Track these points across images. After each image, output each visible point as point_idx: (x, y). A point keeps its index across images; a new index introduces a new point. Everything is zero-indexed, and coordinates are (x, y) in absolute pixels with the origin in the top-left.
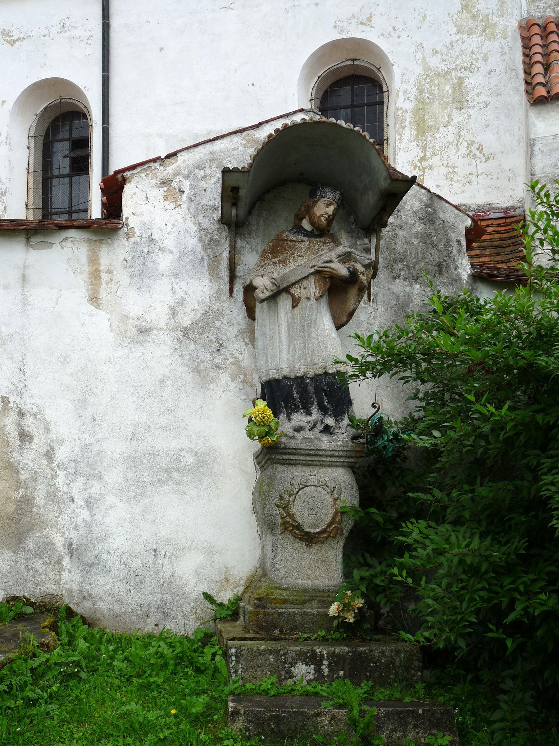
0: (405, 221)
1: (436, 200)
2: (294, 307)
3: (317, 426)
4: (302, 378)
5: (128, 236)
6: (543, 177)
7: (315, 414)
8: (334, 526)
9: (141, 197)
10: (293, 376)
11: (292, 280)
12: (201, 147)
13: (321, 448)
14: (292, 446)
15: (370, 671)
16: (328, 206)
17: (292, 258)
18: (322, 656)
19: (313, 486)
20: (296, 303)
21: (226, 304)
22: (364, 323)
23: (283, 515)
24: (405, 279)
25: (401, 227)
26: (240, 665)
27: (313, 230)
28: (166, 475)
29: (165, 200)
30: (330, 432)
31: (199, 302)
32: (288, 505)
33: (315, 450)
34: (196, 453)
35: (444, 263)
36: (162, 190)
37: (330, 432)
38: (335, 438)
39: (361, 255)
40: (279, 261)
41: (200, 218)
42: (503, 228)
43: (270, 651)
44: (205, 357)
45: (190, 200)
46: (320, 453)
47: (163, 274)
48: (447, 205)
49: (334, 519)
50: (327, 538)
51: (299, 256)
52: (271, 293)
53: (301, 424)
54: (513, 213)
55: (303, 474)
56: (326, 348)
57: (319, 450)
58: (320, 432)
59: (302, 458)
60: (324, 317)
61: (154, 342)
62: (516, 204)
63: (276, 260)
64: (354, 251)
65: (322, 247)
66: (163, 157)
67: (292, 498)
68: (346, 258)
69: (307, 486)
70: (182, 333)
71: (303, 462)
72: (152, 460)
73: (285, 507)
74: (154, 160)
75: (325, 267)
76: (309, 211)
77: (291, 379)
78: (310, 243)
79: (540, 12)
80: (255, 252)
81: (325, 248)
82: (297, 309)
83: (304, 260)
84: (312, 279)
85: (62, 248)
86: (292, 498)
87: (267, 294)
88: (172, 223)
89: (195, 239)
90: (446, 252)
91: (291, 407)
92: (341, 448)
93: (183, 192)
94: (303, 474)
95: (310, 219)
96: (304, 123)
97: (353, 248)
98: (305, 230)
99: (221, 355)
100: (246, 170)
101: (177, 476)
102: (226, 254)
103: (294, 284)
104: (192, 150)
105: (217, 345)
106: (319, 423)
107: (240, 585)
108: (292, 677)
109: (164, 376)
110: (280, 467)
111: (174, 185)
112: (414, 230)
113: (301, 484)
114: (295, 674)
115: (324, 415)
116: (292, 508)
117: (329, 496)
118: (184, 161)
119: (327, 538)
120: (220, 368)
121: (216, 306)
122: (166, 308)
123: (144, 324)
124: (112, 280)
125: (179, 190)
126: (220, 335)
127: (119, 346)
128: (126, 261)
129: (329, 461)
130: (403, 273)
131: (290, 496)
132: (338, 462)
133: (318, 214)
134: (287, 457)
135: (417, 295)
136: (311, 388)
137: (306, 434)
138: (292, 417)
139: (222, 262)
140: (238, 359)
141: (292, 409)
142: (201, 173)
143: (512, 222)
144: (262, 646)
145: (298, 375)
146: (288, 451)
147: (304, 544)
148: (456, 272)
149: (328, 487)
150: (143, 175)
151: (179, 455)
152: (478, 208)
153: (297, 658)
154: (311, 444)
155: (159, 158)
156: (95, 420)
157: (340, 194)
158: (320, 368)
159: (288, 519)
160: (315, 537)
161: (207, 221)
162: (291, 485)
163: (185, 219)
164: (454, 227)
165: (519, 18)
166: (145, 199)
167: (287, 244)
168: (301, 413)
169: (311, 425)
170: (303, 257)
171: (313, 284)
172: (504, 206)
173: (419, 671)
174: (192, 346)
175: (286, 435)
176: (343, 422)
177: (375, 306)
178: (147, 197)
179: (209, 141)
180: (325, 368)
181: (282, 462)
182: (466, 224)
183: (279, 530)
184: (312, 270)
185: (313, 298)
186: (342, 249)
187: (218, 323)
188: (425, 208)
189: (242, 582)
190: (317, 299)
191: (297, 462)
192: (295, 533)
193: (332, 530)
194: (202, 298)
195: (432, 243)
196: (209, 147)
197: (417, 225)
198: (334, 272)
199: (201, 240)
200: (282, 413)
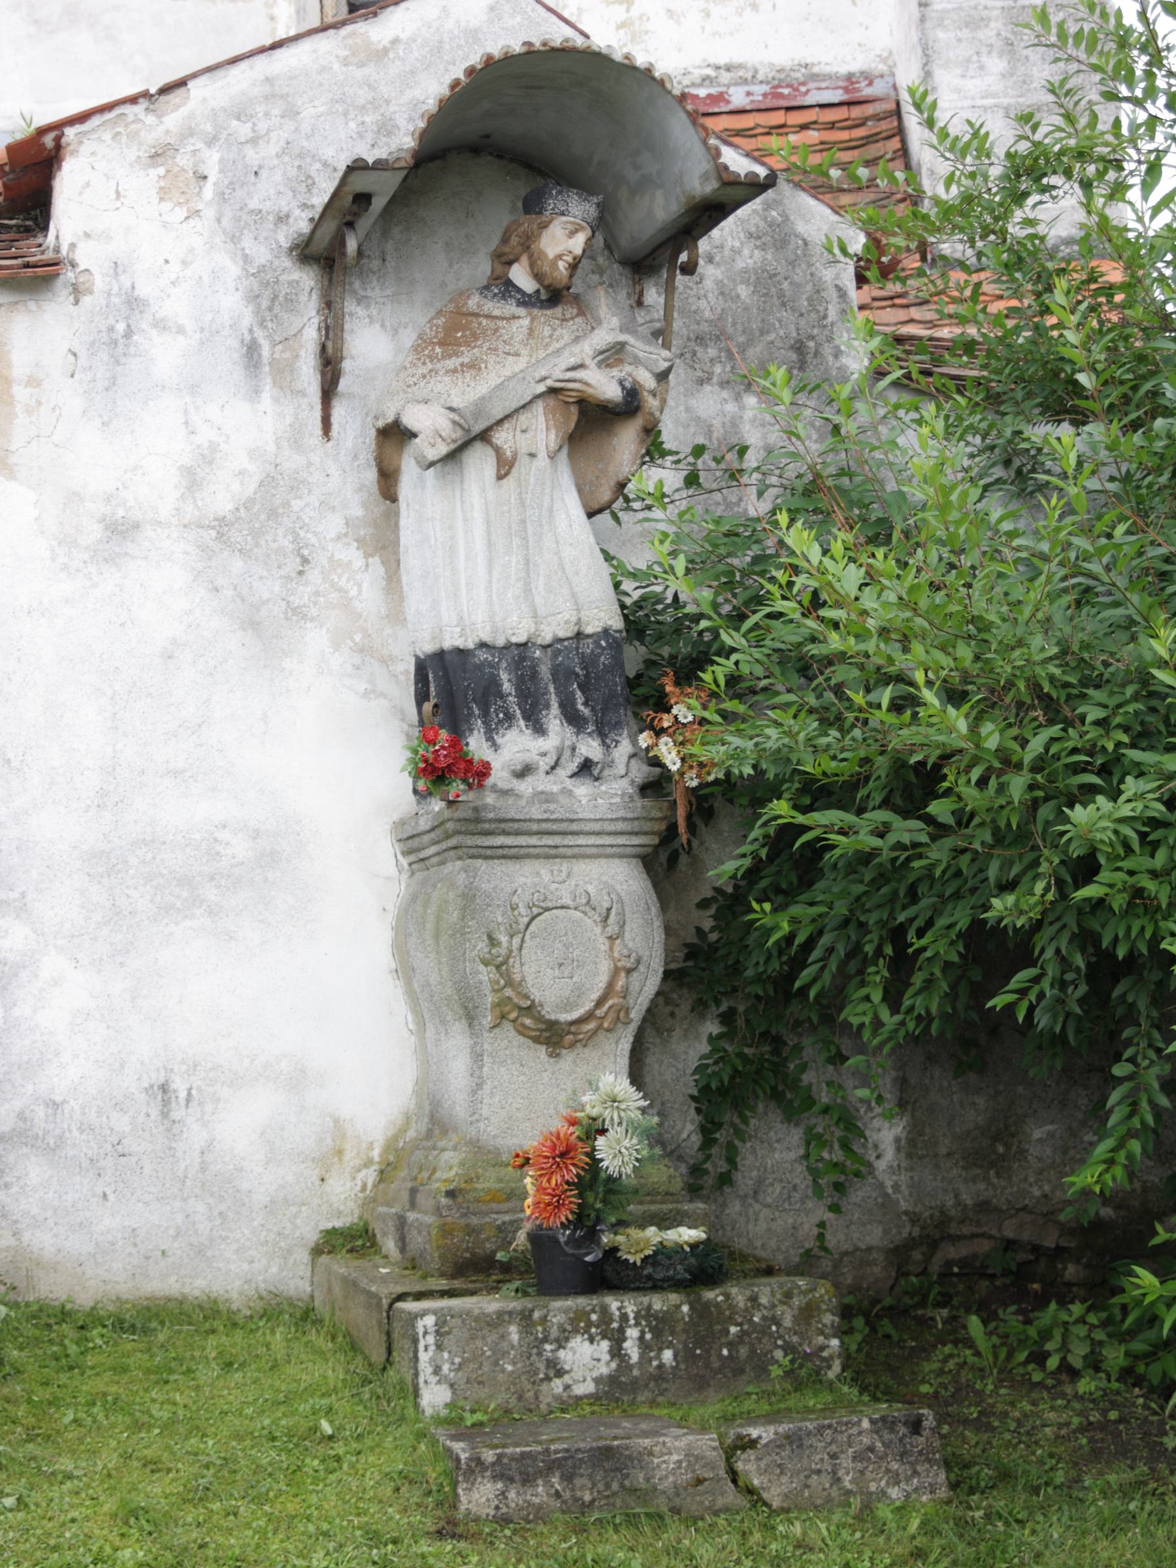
0: (718, 243)
2: (500, 477)
3: (562, 760)
5: (77, 292)
6: (948, 11)
7: (557, 729)
8: (610, 1002)
10: (500, 642)
12: (243, 66)
14: (512, 814)
15: (731, 1345)
16: (572, 233)
17: (492, 359)
18: (624, 1317)
19: (562, 907)
20: (505, 467)
21: (315, 458)
23: (498, 982)
24: (724, 384)
26: (446, 1355)
27: (538, 291)
28: (185, 894)
29: (162, 199)
30: (591, 775)
32: (508, 957)
33: (562, 820)
34: (256, 834)
35: (811, 344)
37: (591, 775)
38: (603, 788)
39: (647, 348)
40: (462, 365)
41: (247, 243)
42: (844, 135)
43: (510, 1313)
45: (222, 197)
46: (575, 827)
49: (610, 985)
50: (595, 1032)
54: (867, 92)
55: (536, 880)
57: (572, 821)
58: (571, 777)
59: (534, 840)
60: (566, 498)
61: (146, 558)
62: (873, 65)
63: (452, 363)
66: (153, 91)
67: (516, 941)
68: (613, 355)
69: (547, 909)
70: (213, 533)
71: (537, 851)
72: (149, 856)
73: (502, 964)
74: (133, 100)
75: (569, 381)
76: (528, 248)
77: (494, 648)
78: (532, 320)
80: (377, 326)
81: (565, 333)
82: (509, 482)
83: (522, 363)
84: (539, 407)
86: (516, 941)
87: (443, 449)
89: (238, 296)
92: (621, 813)
93: (205, 177)
94: (536, 880)
95: (532, 265)
96: (528, 53)
98: (519, 290)
99: (306, 584)
101: (211, 894)
102: (311, 335)
103: (500, 422)
104: (220, 73)
107: (368, 1163)
108: (560, 1373)
109: (174, 642)
111: (183, 160)
112: (740, 264)
114: (567, 1367)
115: (578, 734)
116: (517, 965)
117: (598, 930)
118: (205, 100)
119: (595, 1032)
120: (304, 617)
123: (121, 512)
124: (39, 403)
126: (302, 533)
127: (62, 570)
128: (75, 355)
130: (718, 369)
131: (512, 937)
132: (612, 846)
136: (545, 671)
139: (302, 353)
141: (500, 721)
142: (243, 130)
143: (867, 119)
144: (489, 1304)
145: (514, 640)
146: (506, 825)
147: (542, 1050)
148: (837, 365)
150: (107, 136)
151: (216, 840)
152: (778, 76)
153: (569, 1328)
154: (552, 807)
155: (146, 95)
156: (9, 761)
157: (598, 205)
159: (508, 992)
160: (569, 1033)
161: (263, 249)
166: (114, 196)
169: (550, 760)
170: (517, 355)
171: (542, 419)
172: (844, 70)
173: (835, 1336)
174: (238, 565)
176: (620, 748)
178: (118, 193)
179: (262, 50)
181: (489, 852)
183: (488, 1020)
184: (541, 388)
185: (542, 455)
186: (603, 337)
188: (765, 210)
189: (376, 1154)
190: (552, 457)
191: (523, 851)
192: (523, 1025)
193: (607, 1013)
195: (781, 294)
197: (746, 252)
198: (590, 391)
199: (253, 298)
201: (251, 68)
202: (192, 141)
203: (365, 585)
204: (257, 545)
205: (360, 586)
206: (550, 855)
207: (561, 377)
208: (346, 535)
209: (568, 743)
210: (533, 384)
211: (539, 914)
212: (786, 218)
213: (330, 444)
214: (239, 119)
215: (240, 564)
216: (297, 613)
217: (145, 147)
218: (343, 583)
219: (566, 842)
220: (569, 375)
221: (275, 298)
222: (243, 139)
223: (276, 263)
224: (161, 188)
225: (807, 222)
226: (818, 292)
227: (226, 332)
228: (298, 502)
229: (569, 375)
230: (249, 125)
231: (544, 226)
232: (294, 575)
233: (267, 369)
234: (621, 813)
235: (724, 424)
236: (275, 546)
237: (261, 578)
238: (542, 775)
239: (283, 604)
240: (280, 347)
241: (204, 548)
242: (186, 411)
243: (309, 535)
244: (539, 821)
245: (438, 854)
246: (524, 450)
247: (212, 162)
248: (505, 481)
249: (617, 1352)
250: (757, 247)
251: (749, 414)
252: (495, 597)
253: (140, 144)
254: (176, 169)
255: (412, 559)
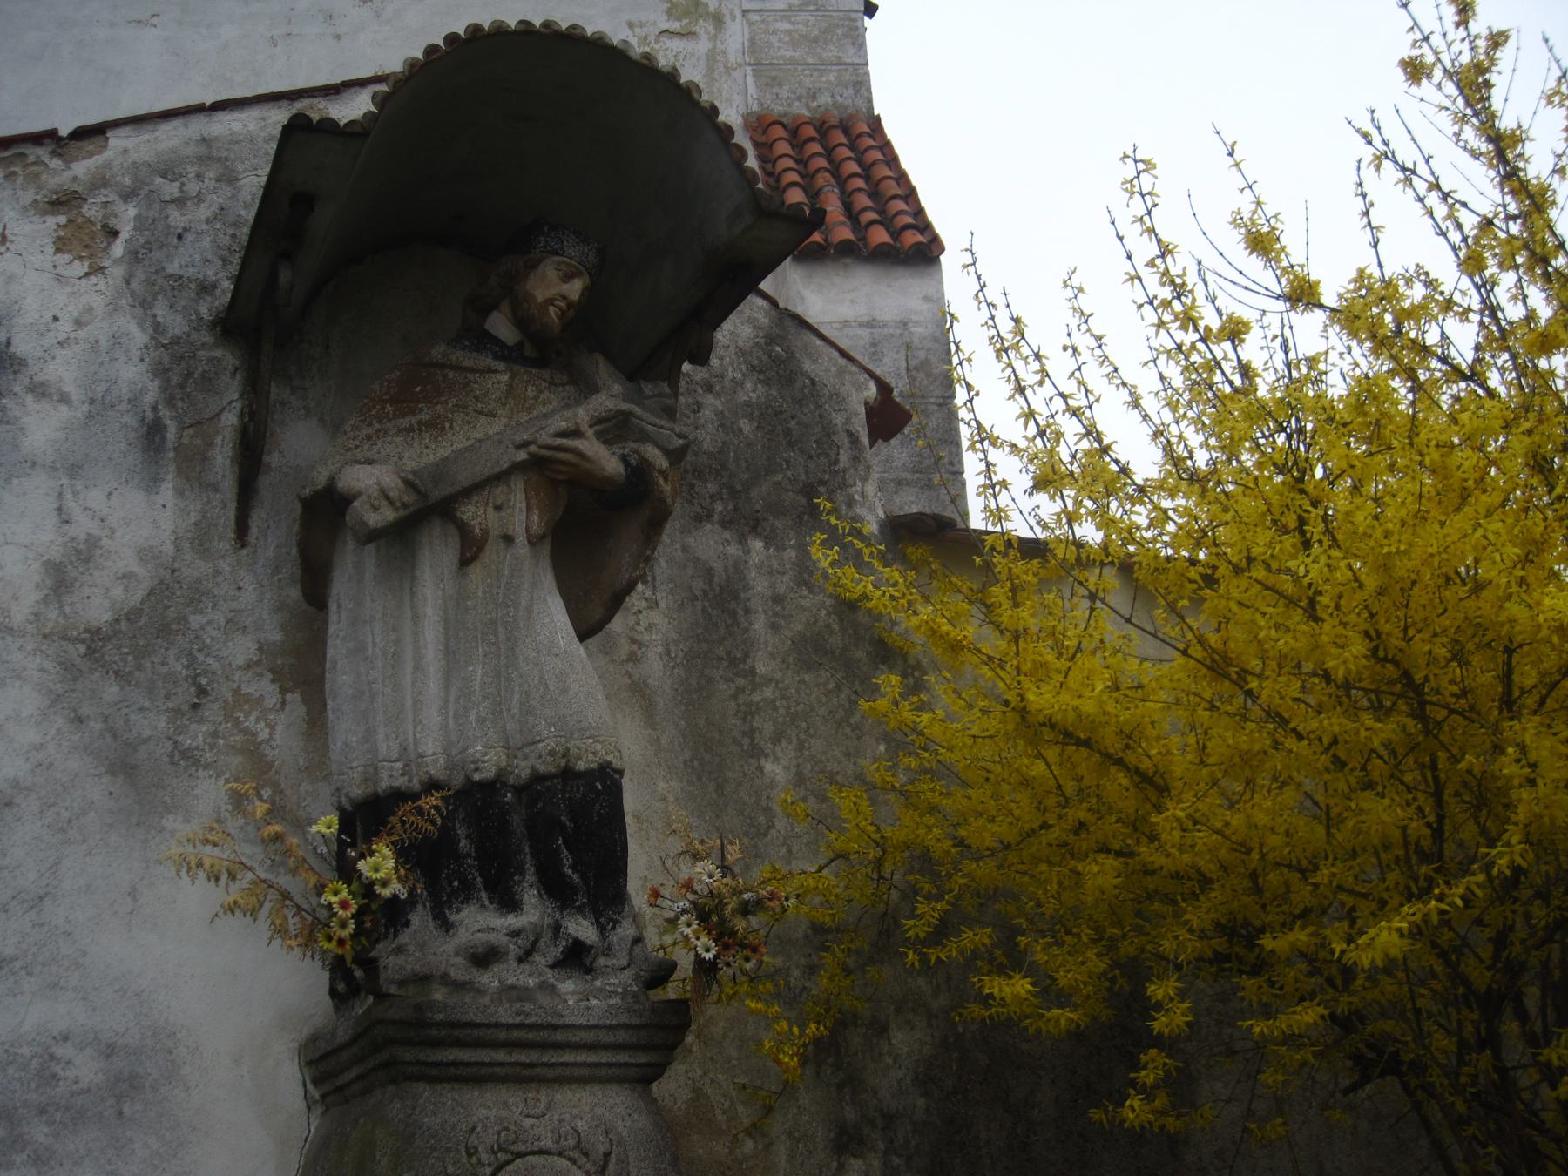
1: (792, 327)
2: (465, 562)
3: (541, 944)
4: (491, 788)
11: (464, 477)
12: (176, 123)
13: (557, 1021)
14: (472, 1015)
16: (568, 277)
19: (541, 1152)
20: (471, 550)
22: (623, 641)
24: (725, 524)
25: (709, 388)
27: (520, 345)
29: (58, 250)
31: (144, 554)
34: (110, 1051)
36: (52, 221)
38: (598, 983)
40: (420, 423)
41: (161, 310)
44: (152, 724)
46: (559, 1037)
47: (34, 463)
48: (819, 342)
51: (481, 413)
52: (402, 513)
53: (492, 938)
55: (503, 1113)
56: (565, 691)
57: (555, 1027)
58: (552, 967)
59: (500, 1056)
60: (550, 600)
63: (404, 422)
64: (638, 411)
65: (547, 393)
70: (82, 649)
74: (37, 139)
78: (513, 376)
79: (782, 105)
82: (476, 572)
83: (496, 427)
84: (518, 484)
87: (388, 515)
88: (75, 314)
89: (142, 367)
90: (823, 459)
91: (450, 883)
92: (624, 1019)
94: (503, 1113)
97: (631, 401)
98: (497, 341)
99: (202, 721)
100: (357, 129)
102: (230, 419)
103: (468, 492)
105: (193, 689)
106: (547, 936)
109: (15, 784)
110: (424, 1091)
111: (91, 211)
112: (742, 397)
113: (501, 1149)
115: (562, 908)
121: (195, 568)
122: (37, 565)
125: (104, 226)
126: (201, 658)
129: (584, 1064)
132: (609, 1065)
133: (540, 298)
134: (451, 1055)
135: (760, 567)
136: (517, 821)
137: (510, 973)
138: (453, 918)
139: (218, 440)
140: (255, 735)
142: (170, 189)
145: (477, 777)
146: (462, 1033)
149: (586, 1155)
151: (52, 1057)
154: (528, 1007)
155: (52, 135)
158: (552, 753)
161: (179, 319)
162: (470, 1155)
163: (113, 308)
164: (838, 399)
165: (742, 110)
167: (445, 376)
168: (483, 906)
170: (492, 415)
174: (112, 691)
175: (445, 980)
177: (648, 594)
180: (566, 754)
181: (434, 1072)
182: (866, 393)
184: (522, 456)
185: (521, 539)
187: (196, 621)
188: (766, 344)
194: (153, 543)
195: (788, 432)
196: (198, 126)
197: (749, 385)
199: (159, 371)
200: (420, 907)
201: (186, 126)
202: (104, 191)
203: (279, 728)
204: (139, 668)
205: (272, 728)
206: (524, 1077)
207: (549, 441)
208: (258, 663)
209: (548, 921)
210: (511, 450)
211: (508, 1162)
212: (792, 356)
213: (244, 552)
214: (164, 176)
215: (115, 689)
216: (187, 759)
217: (45, 192)
218: (250, 723)
219: (546, 1058)
220: (559, 441)
221: (189, 374)
222: (167, 198)
223: (195, 336)
224: (59, 238)
225: (814, 361)
226: (828, 435)
227: (123, 407)
228: (198, 617)
229: (559, 441)
230: (177, 184)
231: (533, 266)
232: (185, 708)
233: (171, 454)
234: (624, 1019)
235: (726, 569)
236: (164, 670)
237: (142, 709)
238: (514, 964)
239: (169, 745)
240: (191, 431)
241: (66, 666)
242: (60, 495)
243: (210, 660)
244: (509, 1027)
245: (360, 1078)
246: (494, 532)
247: (127, 217)
248: (471, 568)
250: (761, 382)
251: (755, 558)
252: (451, 722)
253: (40, 187)
254: (80, 220)
255: (342, 678)
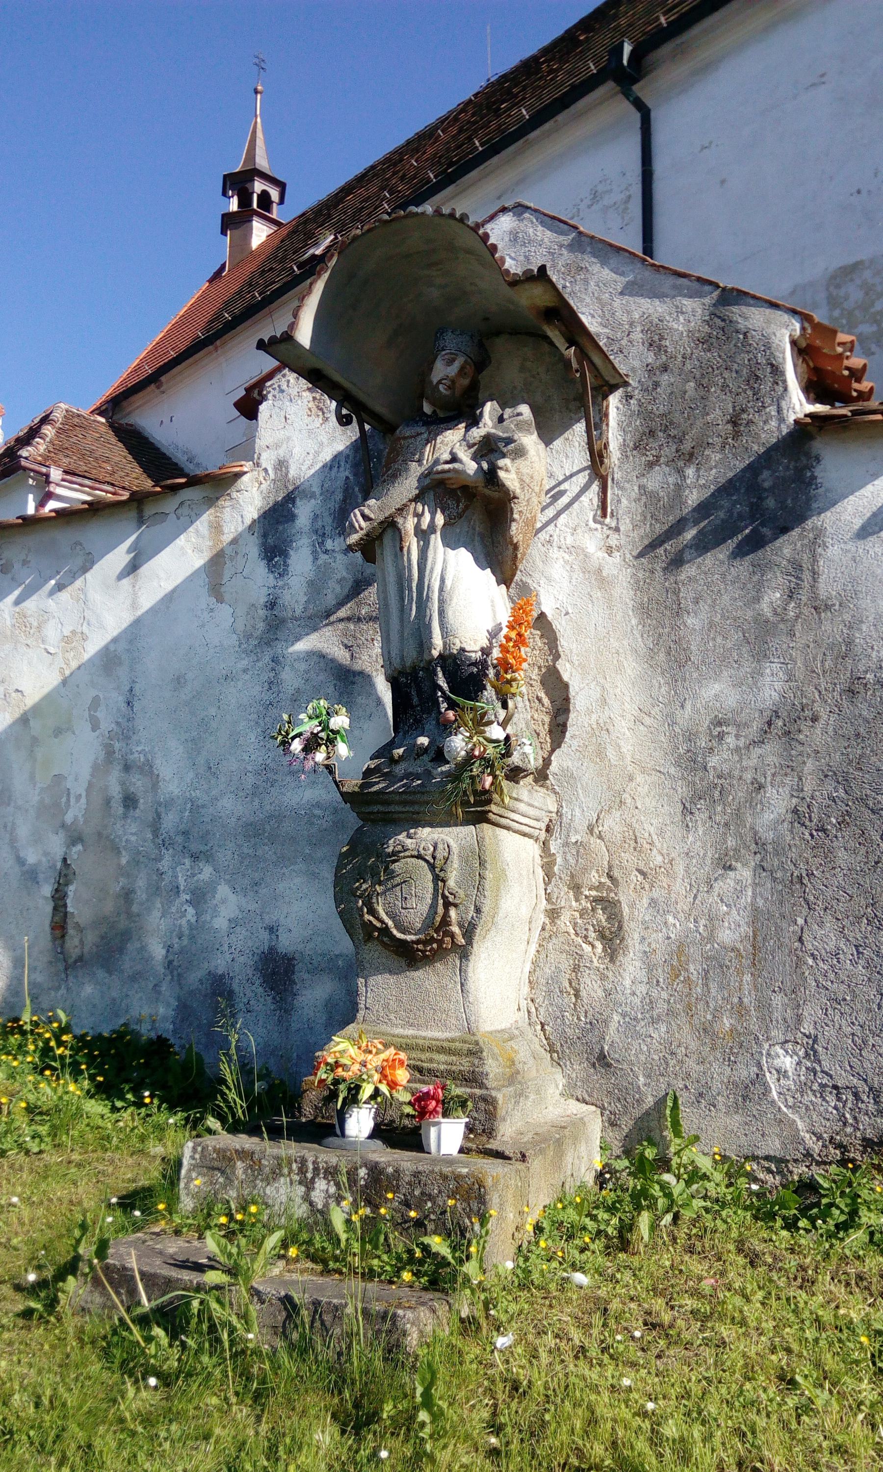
9: (278, 422)
85: (178, 518)
109: (298, 690)
249: (307, 1198)
